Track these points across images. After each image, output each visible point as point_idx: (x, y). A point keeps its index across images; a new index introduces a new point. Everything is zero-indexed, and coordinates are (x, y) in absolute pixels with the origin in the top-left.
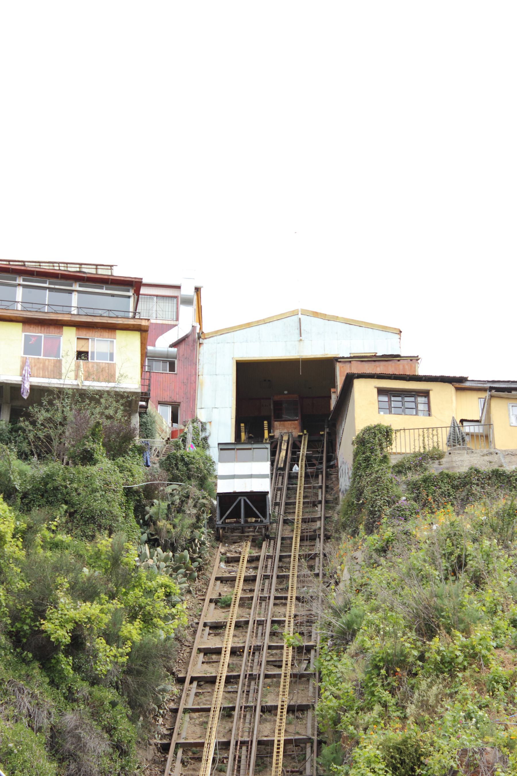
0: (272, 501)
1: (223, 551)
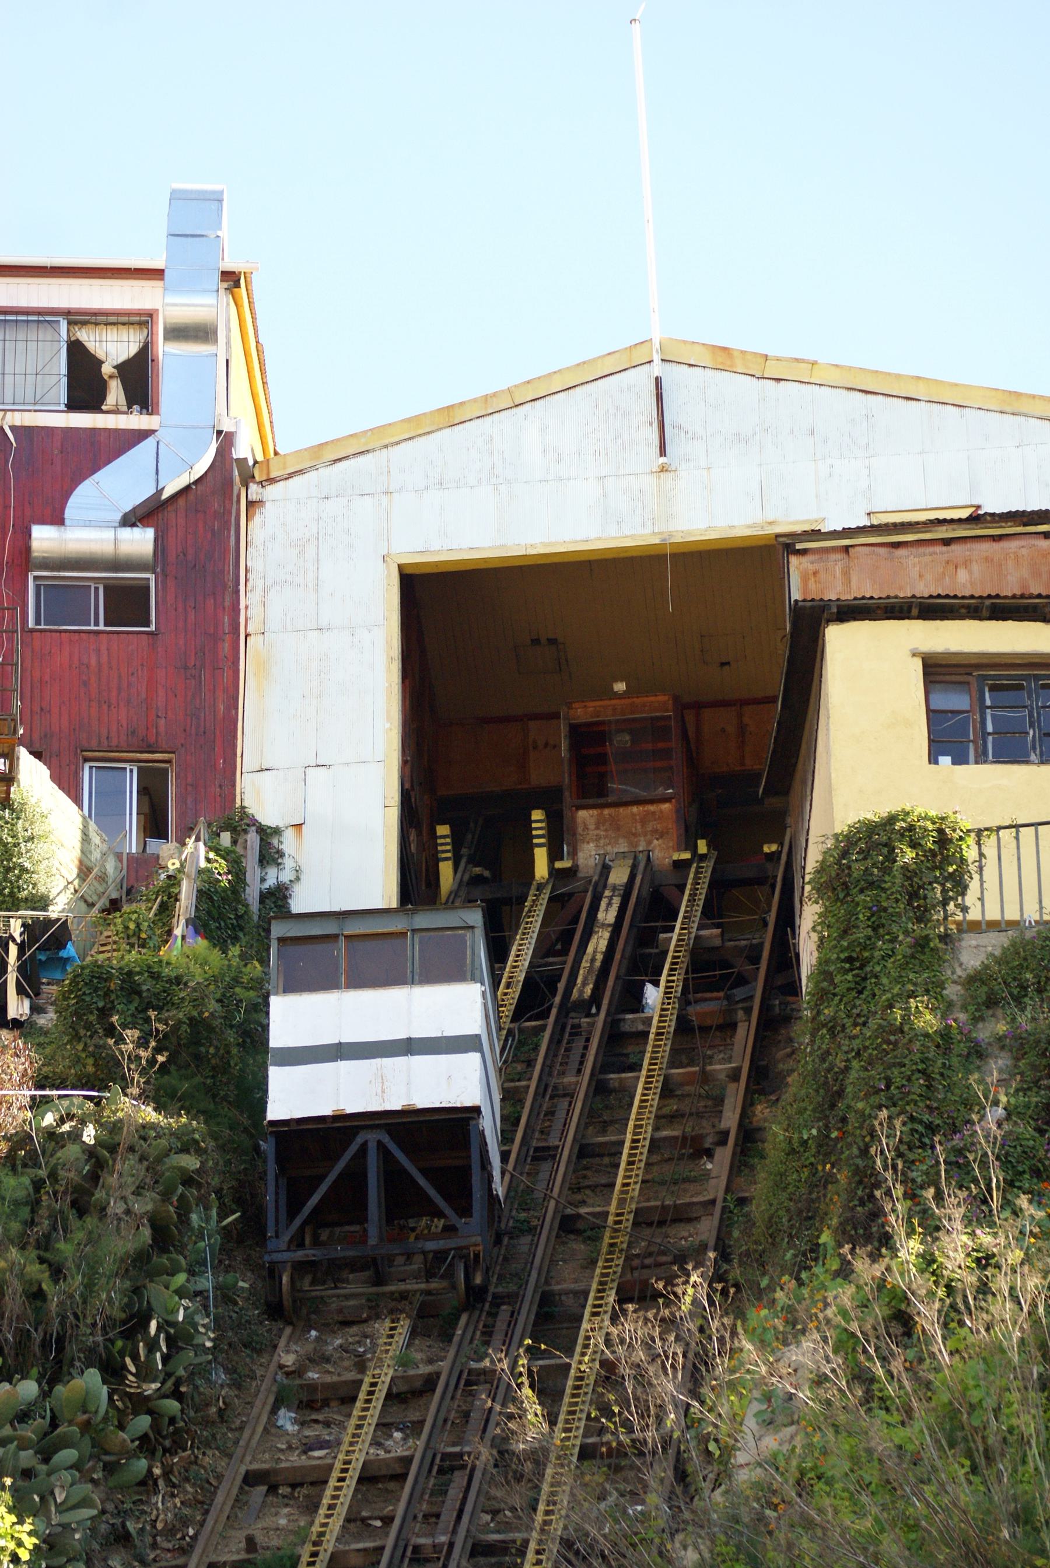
1: (289, 1360)
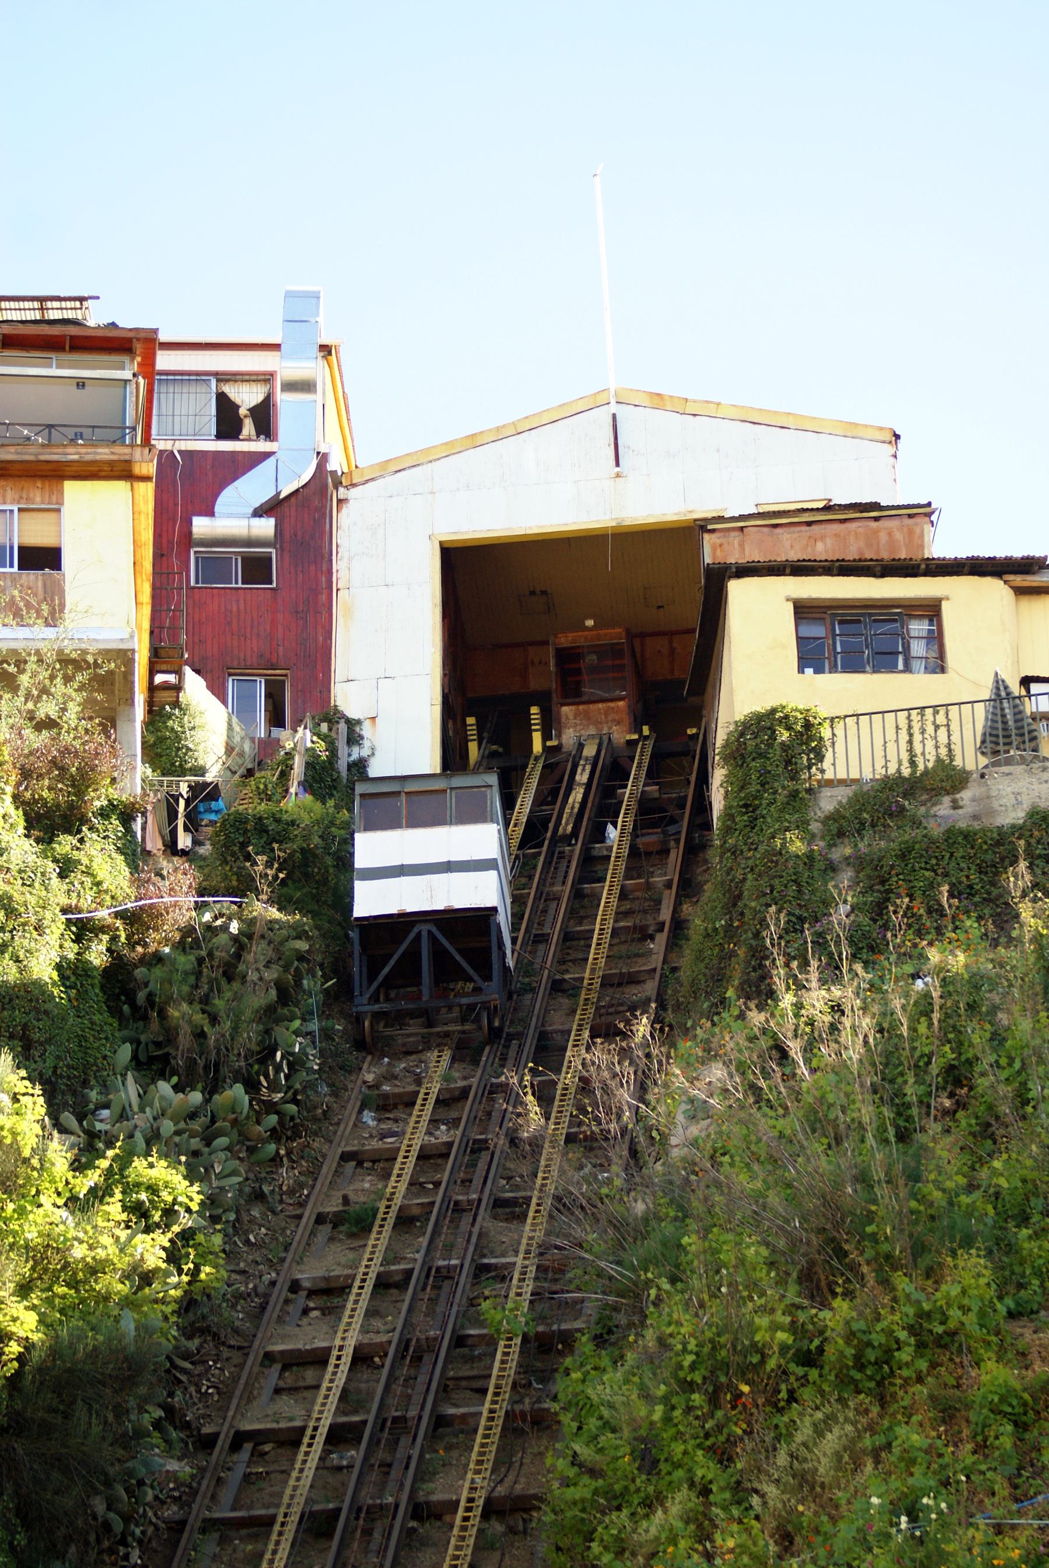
0: (515, 928)
